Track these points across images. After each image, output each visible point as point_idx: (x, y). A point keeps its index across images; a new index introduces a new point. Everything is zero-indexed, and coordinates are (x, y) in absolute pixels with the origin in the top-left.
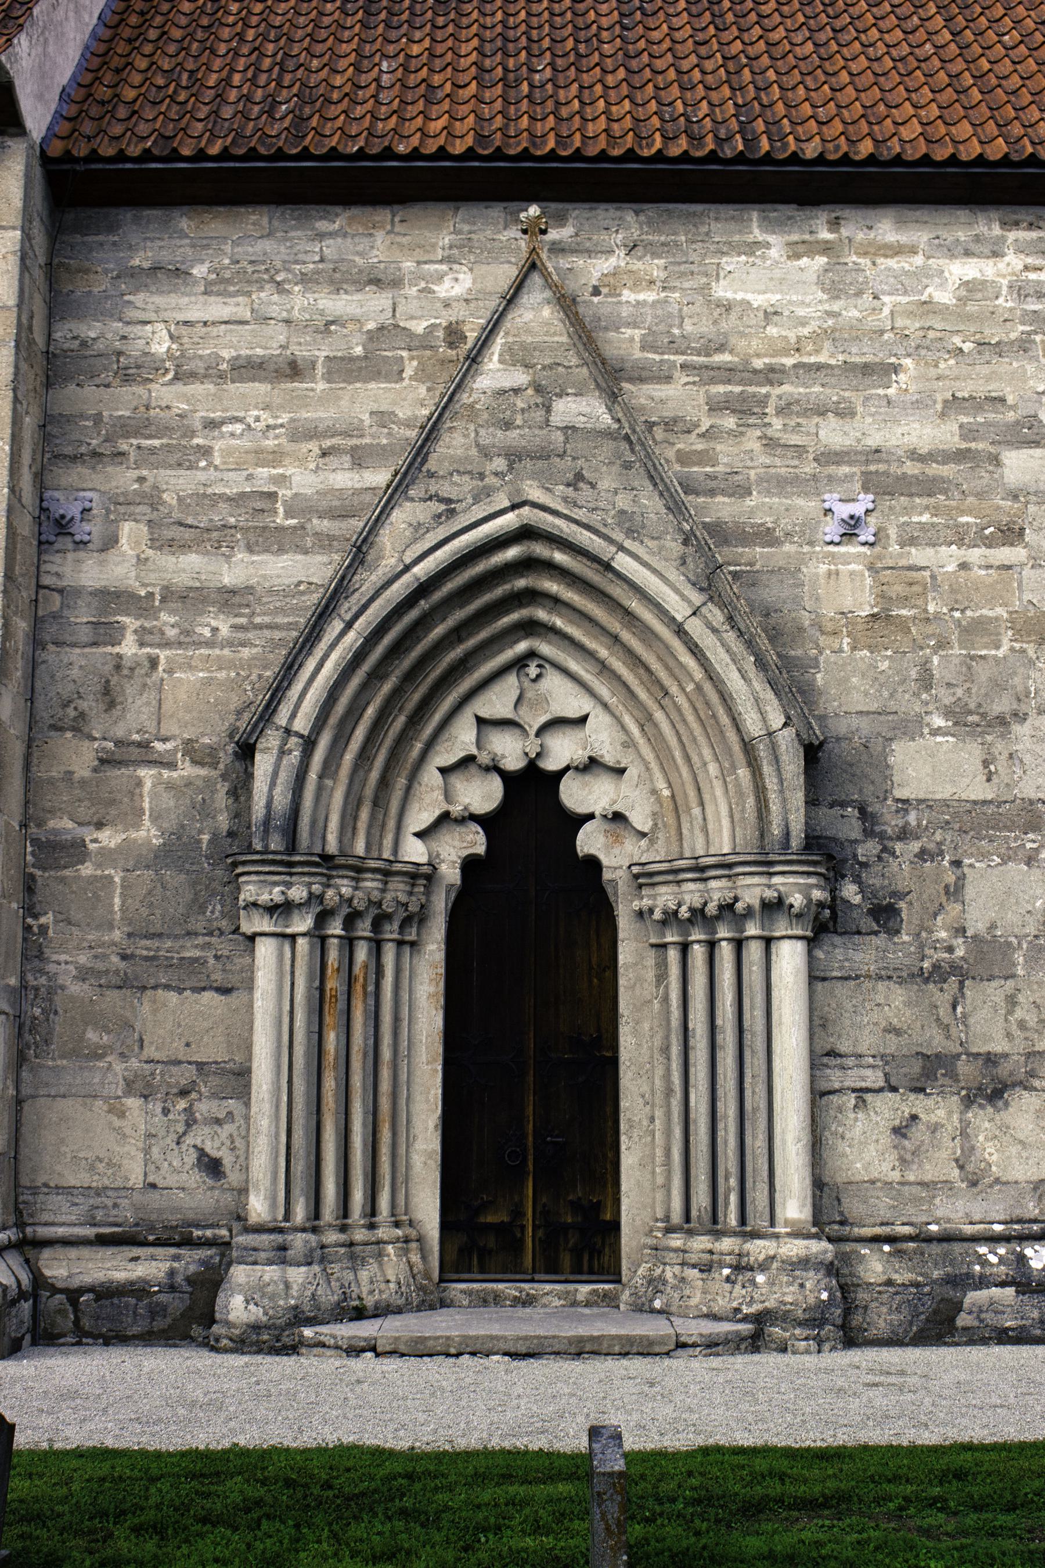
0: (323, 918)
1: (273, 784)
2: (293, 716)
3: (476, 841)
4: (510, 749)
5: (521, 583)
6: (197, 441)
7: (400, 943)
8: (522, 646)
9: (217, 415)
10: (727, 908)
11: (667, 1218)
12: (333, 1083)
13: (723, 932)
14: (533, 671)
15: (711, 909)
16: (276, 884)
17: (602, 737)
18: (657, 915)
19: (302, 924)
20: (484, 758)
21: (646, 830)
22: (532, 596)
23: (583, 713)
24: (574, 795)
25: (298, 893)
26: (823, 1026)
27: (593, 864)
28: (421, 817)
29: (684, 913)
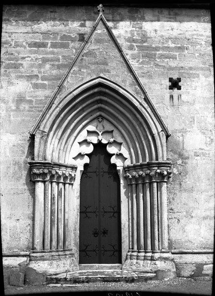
0: (52, 176)
3: (87, 160)
4: (94, 139)
6: (19, 62)
9: (25, 56)
16: (41, 168)
19: (48, 178)
27: (115, 166)
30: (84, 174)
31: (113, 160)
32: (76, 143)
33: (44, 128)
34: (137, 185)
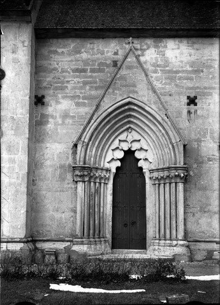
0: (91, 177)
3: (119, 164)
5: (128, 113)
7: (104, 183)
8: (128, 126)
10: (168, 176)
11: (156, 237)
12: (215, 185)
14: (130, 131)
15: (159, 177)
19: (87, 179)
20: (120, 148)
22: (130, 116)
24: (138, 155)
25: (86, 173)
28: (108, 159)
29: (159, 177)
30: (116, 176)
31: (140, 164)
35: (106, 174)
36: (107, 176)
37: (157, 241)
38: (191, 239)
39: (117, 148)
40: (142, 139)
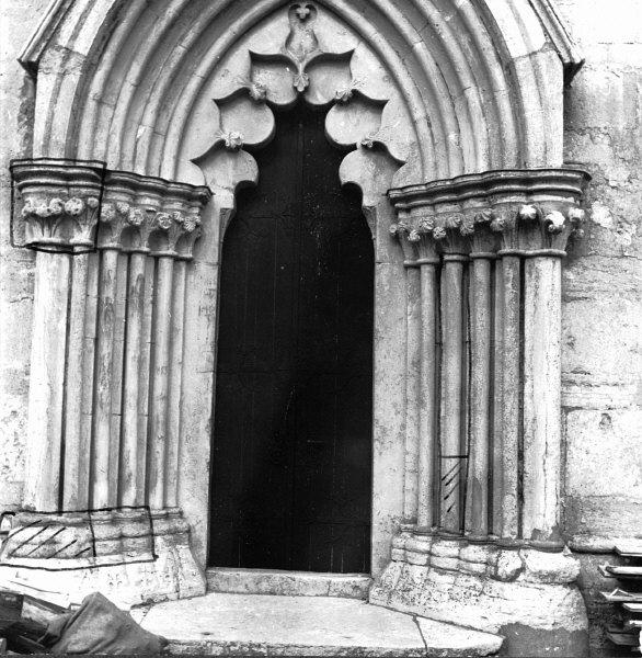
0: (101, 229)
1: (54, 101)
2: (74, 37)
3: (248, 170)
4: (277, 86)
7: (176, 260)
10: (483, 227)
11: (415, 521)
13: (477, 251)
15: (439, 232)
16: (52, 195)
17: (366, 75)
18: (413, 236)
19: (82, 236)
21: (402, 159)
23: (348, 50)
24: (340, 127)
25: (74, 206)
26: (571, 344)
27: (354, 191)
29: (439, 232)
32: (207, 106)
33: (74, 37)
34: (439, 269)
35: (185, 214)
36: (190, 227)
37: (423, 543)
38: (596, 543)
39: (243, 94)
40: (361, 52)
